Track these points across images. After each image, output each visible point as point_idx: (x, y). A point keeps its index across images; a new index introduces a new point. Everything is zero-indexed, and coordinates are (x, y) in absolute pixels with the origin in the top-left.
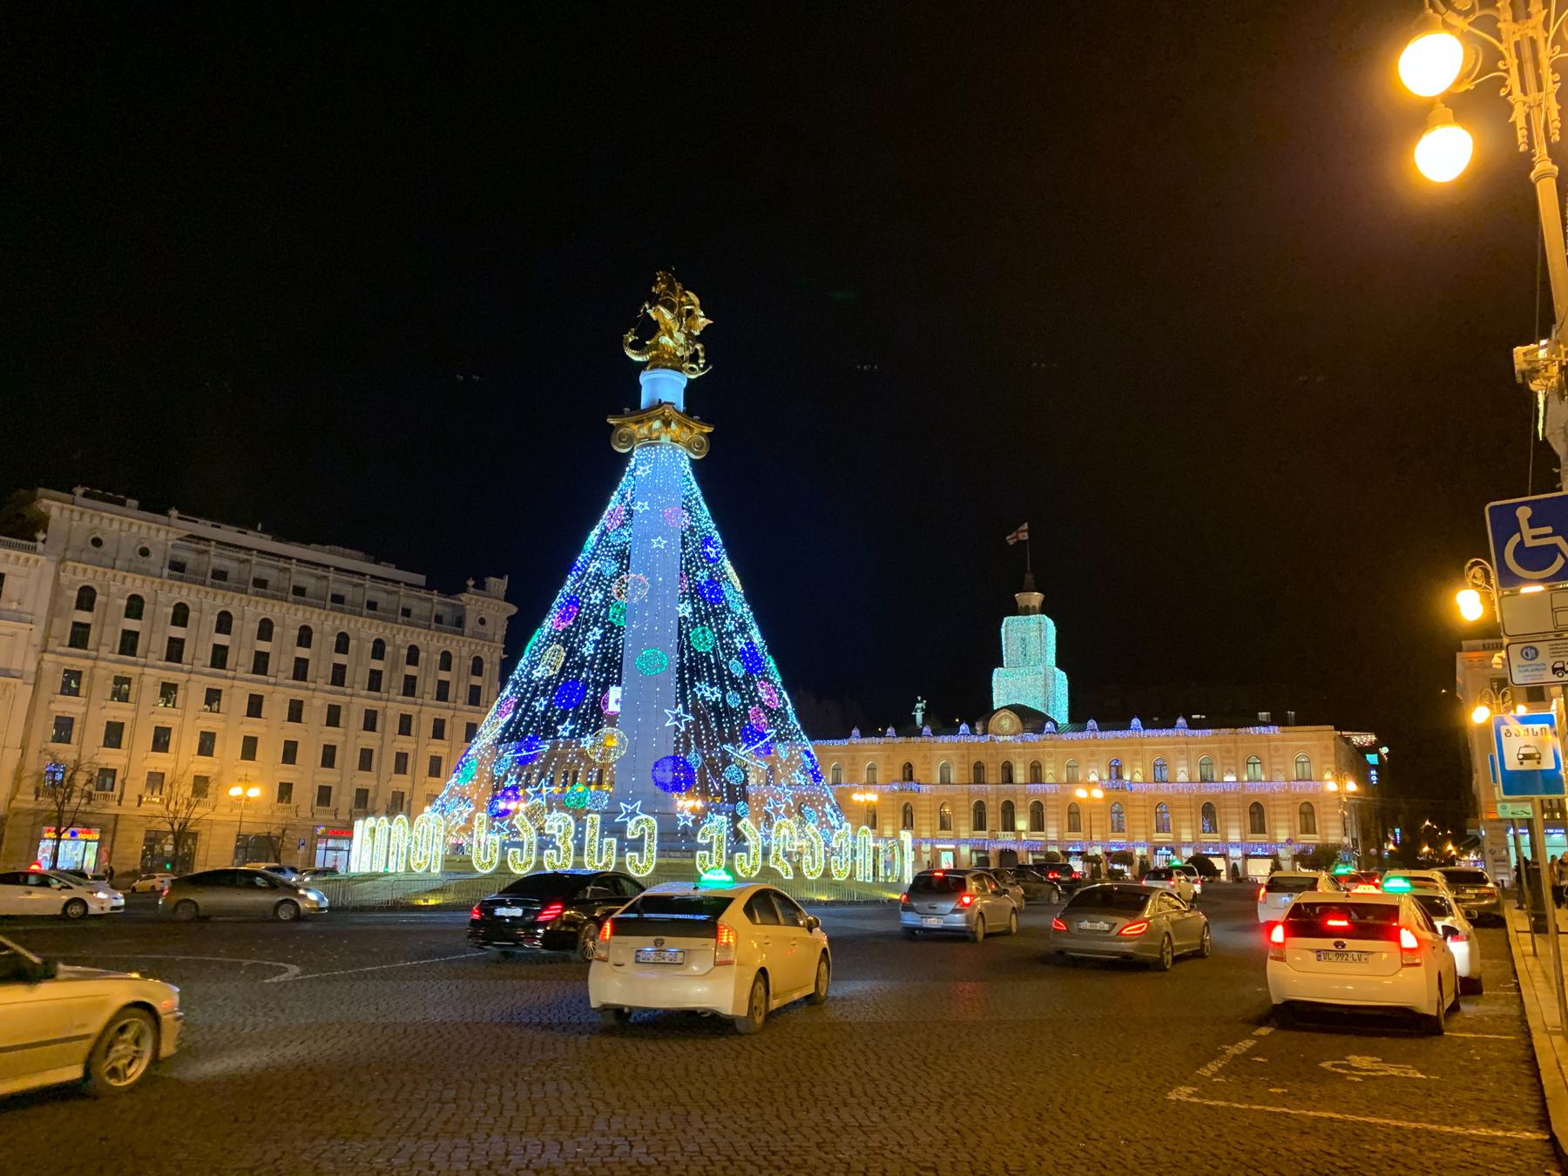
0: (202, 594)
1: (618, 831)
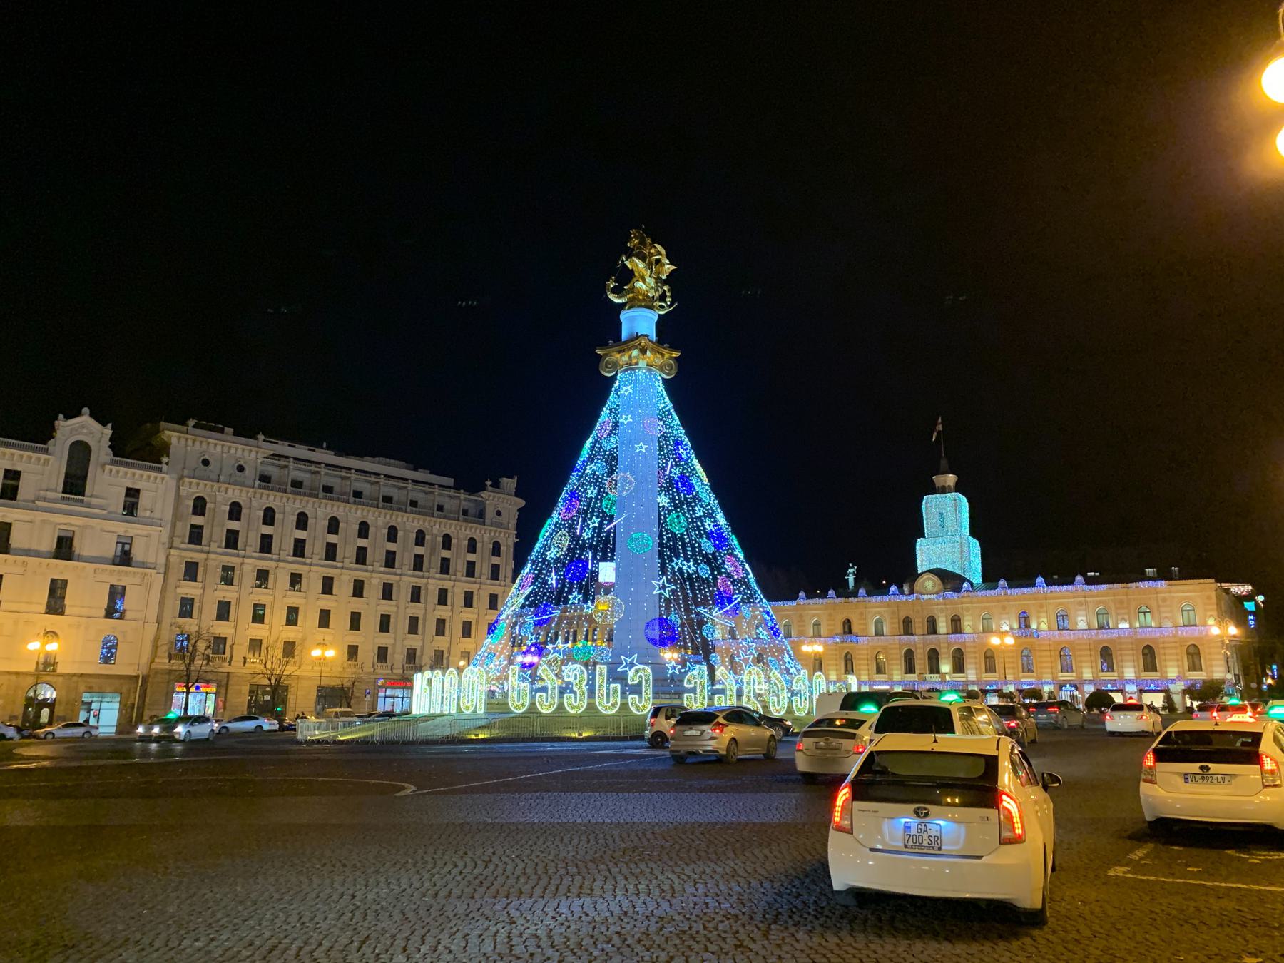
0: (285, 500)
1: (622, 678)
